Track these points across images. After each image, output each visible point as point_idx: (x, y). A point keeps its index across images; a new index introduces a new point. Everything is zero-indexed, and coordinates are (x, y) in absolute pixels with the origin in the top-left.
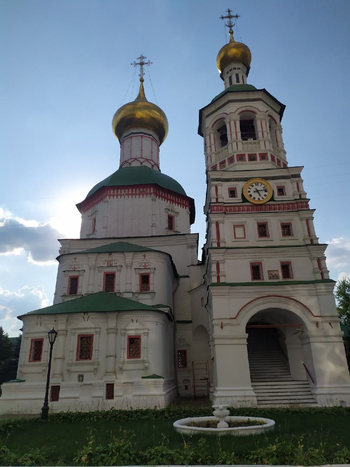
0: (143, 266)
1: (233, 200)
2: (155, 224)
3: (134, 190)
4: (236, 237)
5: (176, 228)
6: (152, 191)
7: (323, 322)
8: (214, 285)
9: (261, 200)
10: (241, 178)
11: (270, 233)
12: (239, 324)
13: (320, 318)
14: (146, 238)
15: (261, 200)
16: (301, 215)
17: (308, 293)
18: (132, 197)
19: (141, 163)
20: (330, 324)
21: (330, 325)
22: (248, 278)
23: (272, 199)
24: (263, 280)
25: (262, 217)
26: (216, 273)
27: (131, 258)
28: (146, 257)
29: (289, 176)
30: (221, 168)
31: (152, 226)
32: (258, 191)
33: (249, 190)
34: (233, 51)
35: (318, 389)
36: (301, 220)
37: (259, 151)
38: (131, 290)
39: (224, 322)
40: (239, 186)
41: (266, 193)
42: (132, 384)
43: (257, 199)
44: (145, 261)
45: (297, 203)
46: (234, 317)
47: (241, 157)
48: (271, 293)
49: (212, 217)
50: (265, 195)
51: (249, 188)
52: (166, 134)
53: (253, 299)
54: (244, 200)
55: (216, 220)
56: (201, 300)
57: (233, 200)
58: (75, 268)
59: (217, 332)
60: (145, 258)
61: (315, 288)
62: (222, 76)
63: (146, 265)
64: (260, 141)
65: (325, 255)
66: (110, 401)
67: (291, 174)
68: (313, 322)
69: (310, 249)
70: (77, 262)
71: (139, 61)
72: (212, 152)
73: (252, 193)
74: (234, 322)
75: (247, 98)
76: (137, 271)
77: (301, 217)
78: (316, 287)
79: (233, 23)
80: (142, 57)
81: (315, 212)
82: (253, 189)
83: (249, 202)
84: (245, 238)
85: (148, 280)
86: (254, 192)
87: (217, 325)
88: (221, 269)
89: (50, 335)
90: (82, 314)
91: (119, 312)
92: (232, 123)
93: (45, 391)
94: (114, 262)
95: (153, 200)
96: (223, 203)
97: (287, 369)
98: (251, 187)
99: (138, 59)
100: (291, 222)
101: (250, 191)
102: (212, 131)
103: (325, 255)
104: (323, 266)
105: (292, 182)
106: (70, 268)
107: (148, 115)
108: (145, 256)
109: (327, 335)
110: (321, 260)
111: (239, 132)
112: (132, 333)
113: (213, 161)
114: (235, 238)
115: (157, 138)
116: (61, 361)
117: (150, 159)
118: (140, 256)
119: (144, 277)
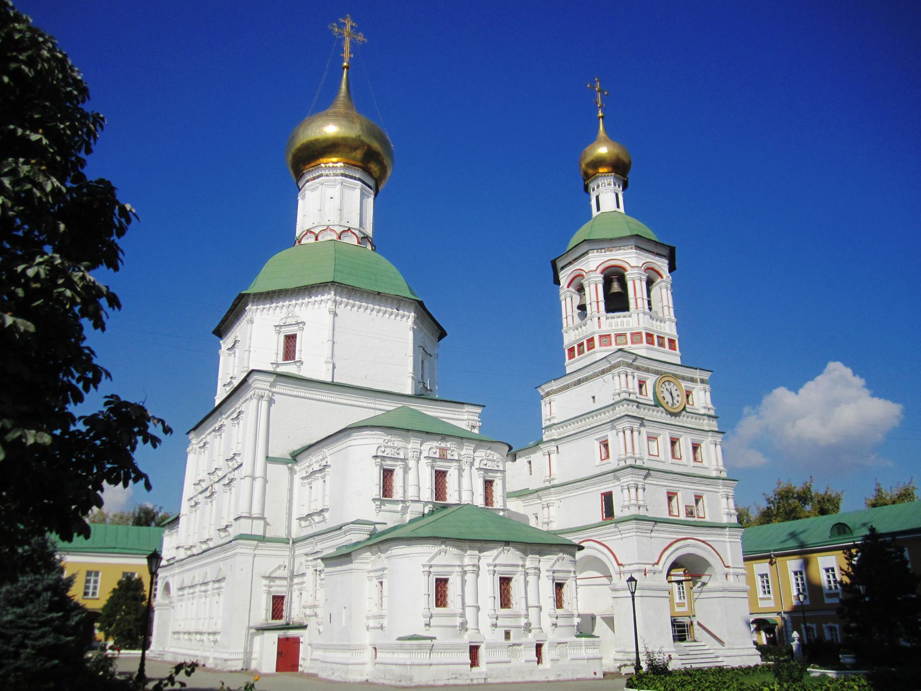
53: (674, 540)
66: (475, 669)
89: (629, 583)
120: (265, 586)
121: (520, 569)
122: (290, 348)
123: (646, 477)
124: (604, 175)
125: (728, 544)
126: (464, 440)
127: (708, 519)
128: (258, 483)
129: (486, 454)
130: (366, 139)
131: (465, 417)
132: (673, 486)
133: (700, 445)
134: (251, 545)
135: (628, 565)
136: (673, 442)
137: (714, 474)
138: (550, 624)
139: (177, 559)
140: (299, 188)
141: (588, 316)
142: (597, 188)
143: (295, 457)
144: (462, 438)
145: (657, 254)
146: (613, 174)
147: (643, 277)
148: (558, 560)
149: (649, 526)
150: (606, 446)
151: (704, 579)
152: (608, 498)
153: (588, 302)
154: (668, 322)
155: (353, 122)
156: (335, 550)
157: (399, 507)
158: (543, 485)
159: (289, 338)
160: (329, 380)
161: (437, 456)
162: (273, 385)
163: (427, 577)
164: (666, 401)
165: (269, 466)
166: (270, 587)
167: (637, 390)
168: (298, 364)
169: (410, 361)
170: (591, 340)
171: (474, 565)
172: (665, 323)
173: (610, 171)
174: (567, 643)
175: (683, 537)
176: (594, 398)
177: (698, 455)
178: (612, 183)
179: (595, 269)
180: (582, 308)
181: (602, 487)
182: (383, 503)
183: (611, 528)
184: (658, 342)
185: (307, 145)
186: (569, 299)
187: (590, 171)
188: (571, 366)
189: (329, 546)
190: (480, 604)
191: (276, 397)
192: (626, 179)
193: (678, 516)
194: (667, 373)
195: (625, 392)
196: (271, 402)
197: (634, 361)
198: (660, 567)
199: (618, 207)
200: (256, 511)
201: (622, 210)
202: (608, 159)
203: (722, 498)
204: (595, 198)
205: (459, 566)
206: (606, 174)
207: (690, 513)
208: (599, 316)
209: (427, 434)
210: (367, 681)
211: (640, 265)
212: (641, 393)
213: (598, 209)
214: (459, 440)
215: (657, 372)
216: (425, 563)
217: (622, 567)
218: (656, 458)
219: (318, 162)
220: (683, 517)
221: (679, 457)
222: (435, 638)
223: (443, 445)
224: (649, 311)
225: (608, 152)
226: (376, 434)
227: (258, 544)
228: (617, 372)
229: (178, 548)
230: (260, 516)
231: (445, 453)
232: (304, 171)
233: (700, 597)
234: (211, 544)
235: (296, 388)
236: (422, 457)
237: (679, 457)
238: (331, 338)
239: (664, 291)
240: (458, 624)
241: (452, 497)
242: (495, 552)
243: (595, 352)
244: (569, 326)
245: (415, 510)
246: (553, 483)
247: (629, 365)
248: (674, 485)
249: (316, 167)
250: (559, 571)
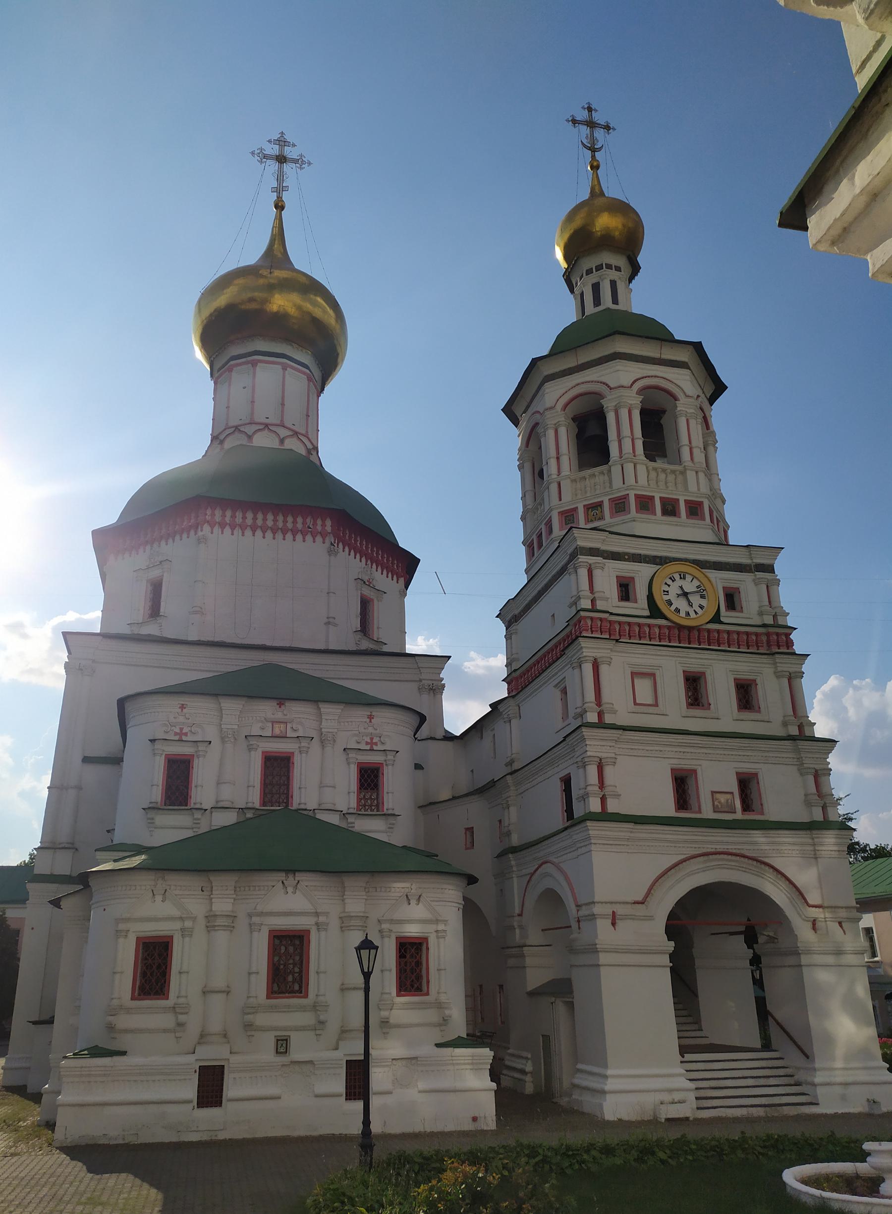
0: (367, 743)
1: (627, 608)
2: (334, 618)
3: (290, 519)
4: (637, 702)
5: (375, 633)
6: (329, 528)
7: (827, 919)
8: (592, 817)
9: (680, 615)
10: (646, 556)
11: (711, 701)
12: (650, 918)
13: (821, 910)
15: (671, 608)
16: (778, 665)
17: (801, 850)
18: (294, 537)
19: (282, 441)
20: (840, 923)
21: (841, 926)
22: (667, 806)
23: (716, 619)
24: (700, 812)
25: (696, 660)
26: (597, 788)
27: (337, 718)
28: (372, 720)
29: (751, 565)
30: (588, 520)
31: (328, 623)
32: (685, 594)
33: (666, 588)
34: (605, 222)
35: (818, 1073)
36: (778, 677)
37: (686, 495)
38: (335, 805)
39: (620, 910)
40: (642, 573)
41: (704, 602)
42: (414, 1061)
43: (683, 614)
44: (371, 730)
45: (768, 635)
46: (640, 899)
47: (645, 504)
48: (720, 848)
49: (585, 645)
50: (701, 607)
51: (666, 584)
52: (338, 369)
54: (655, 611)
55: (594, 655)
56: (464, 832)
57: (627, 608)
58: (181, 733)
59: (604, 933)
60: (370, 722)
61: (810, 841)
62: (568, 277)
63: (374, 741)
64: (685, 470)
65: (829, 763)
67: (754, 561)
68: (806, 919)
69: (802, 749)
70: (187, 715)
71: (274, 150)
72: (562, 474)
73: (672, 596)
74: (640, 910)
75: (657, 355)
76: (352, 755)
77: (779, 669)
78: (813, 839)
79: (598, 141)
80: (282, 142)
81: (808, 660)
82: (674, 590)
83: (666, 618)
84: (656, 705)
85: (360, 780)
86: (679, 595)
87: (603, 916)
88: (608, 781)
90: (282, 876)
91: (372, 873)
92: (624, 413)
94: (289, 726)
95: (331, 552)
96: (608, 615)
97: (690, 1016)
98: (669, 582)
99: (270, 141)
100: (755, 677)
101: (667, 592)
102: (563, 419)
103: (829, 763)
104: (825, 790)
105: (756, 583)
106: (167, 732)
107: (299, 308)
108: (371, 717)
109: (841, 949)
110: (821, 774)
111: (640, 438)
112: (412, 930)
113: (567, 496)
114: (635, 703)
115: (317, 374)
116: (222, 996)
117: (304, 432)
118: (359, 714)
119: (366, 771)
208: (558, 480)
220: (707, 813)
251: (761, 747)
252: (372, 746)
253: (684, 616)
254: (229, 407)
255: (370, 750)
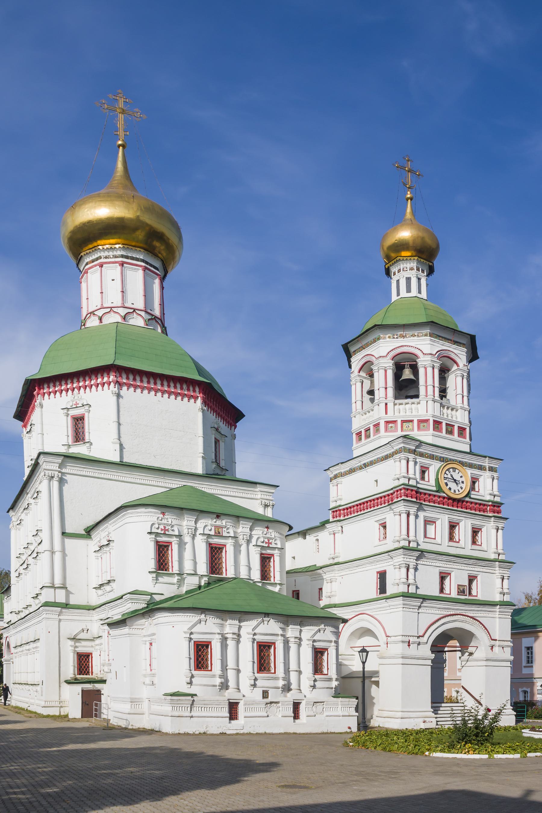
14: (228, 481)
22: (436, 592)
43: (452, 491)
53: (442, 616)
89: (361, 653)
93: (186, 570)
120: (71, 646)
121: (280, 637)
122: (80, 430)
123: (418, 558)
124: (407, 259)
125: (498, 619)
126: (240, 519)
127: (480, 597)
128: (58, 557)
129: (263, 533)
130: (148, 219)
131: (259, 496)
132: (446, 566)
133: (481, 529)
134: (55, 611)
135: (394, 636)
136: (453, 526)
137: (493, 556)
138: (308, 686)
139: (12, 622)
140: (80, 271)
141: (376, 401)
142: (398, 272)
143: (89, 532)
144: (238, 517)
145: (455, 342)
146: (416, 258)
147: (435, 365)
148: (319, 630)
149: (417, 602)
150: (385, 527)
151: (470, 649)
152: (382, 576)
153: (376, 388)
154: (459, 411)
155: (129, 202)
156: (121, 616)
157: (175, 579)
158: (328, 562)
159: (78, 420)
160: (117, 459)
161: (212, 533)
162: (61, 466)
163: (188, 642)
164: (448, 487)
165: (68, 541)
166: (76, 647)
167: (418, 476)
168: (88, 445)
169: (200, 441)
170: (377, 425)
171: (234, 634)
172: (457, 410)
173: (414, 254)
174: (324, 702)
175: (452, 613)
176: (376, 481)
177: (478, 538)
178: (415, 268)
179: (385, 355)
180: (371, 392)
181: (378, 566)
182: (158, 575)
183: (383, 603)
184: (447, 430)
185: (79, 227)
186: (359, 385)
187: (393, 255)
188: (358, 449)
189: (116, 614)
190: (240, 668)
191: (67, 477)
192: (431, 264)
193: (450, 594)
194: (453, 460)
195: (404, 477)
196: (62, 482)
197: (417, 447)
198: (425, 639)
199: (420, 292)
200: (58, 582)
201: (424, 295)
202: (411, 243)
203: (497, 578)
204: (395, 282)
205: (219, 634)
206: (409, 258)
207: (461, 591)
208: (386, 402)
209: (201, 513)
210: (265, 733)
211: (434, 353)
212: (423, 478)
213: (398, 294)
214: (234, 519)
215: (442, 459)
216: (186, 630)
217: (389, 638)
218: (433, 541)
219: (95, 244)
220: (454, 594)
221: (458, 541)
222: (196, 695)
223: (219, 523)
224: (439, 399)
225: (412, 236)
226: (124, 515)
227: (61, 610)
228: (398, 457)
229: (11, 613)
230: (62, 586)
231: (220, 530)
232: (82, 254)
233: (466, 665)
234: (31, 610)
235: (85, 468)
236: (198, 533)
237: (458, 541)
238: (116, 420)
239: (459, 379)
240: (218, 684)
241: (229, 572)
242: (254, 623)
243: (380, 437)
244: (358, 411)
245: (191, 582)
246: (336, 561)
247: (414, 452)
248: (449, 566)
249: (93, 249)
250: (319, 641)
251: (437, 558)
252: (268, 545)
253: (453, 492)
254: (88, 299)
255: (267, 547)
